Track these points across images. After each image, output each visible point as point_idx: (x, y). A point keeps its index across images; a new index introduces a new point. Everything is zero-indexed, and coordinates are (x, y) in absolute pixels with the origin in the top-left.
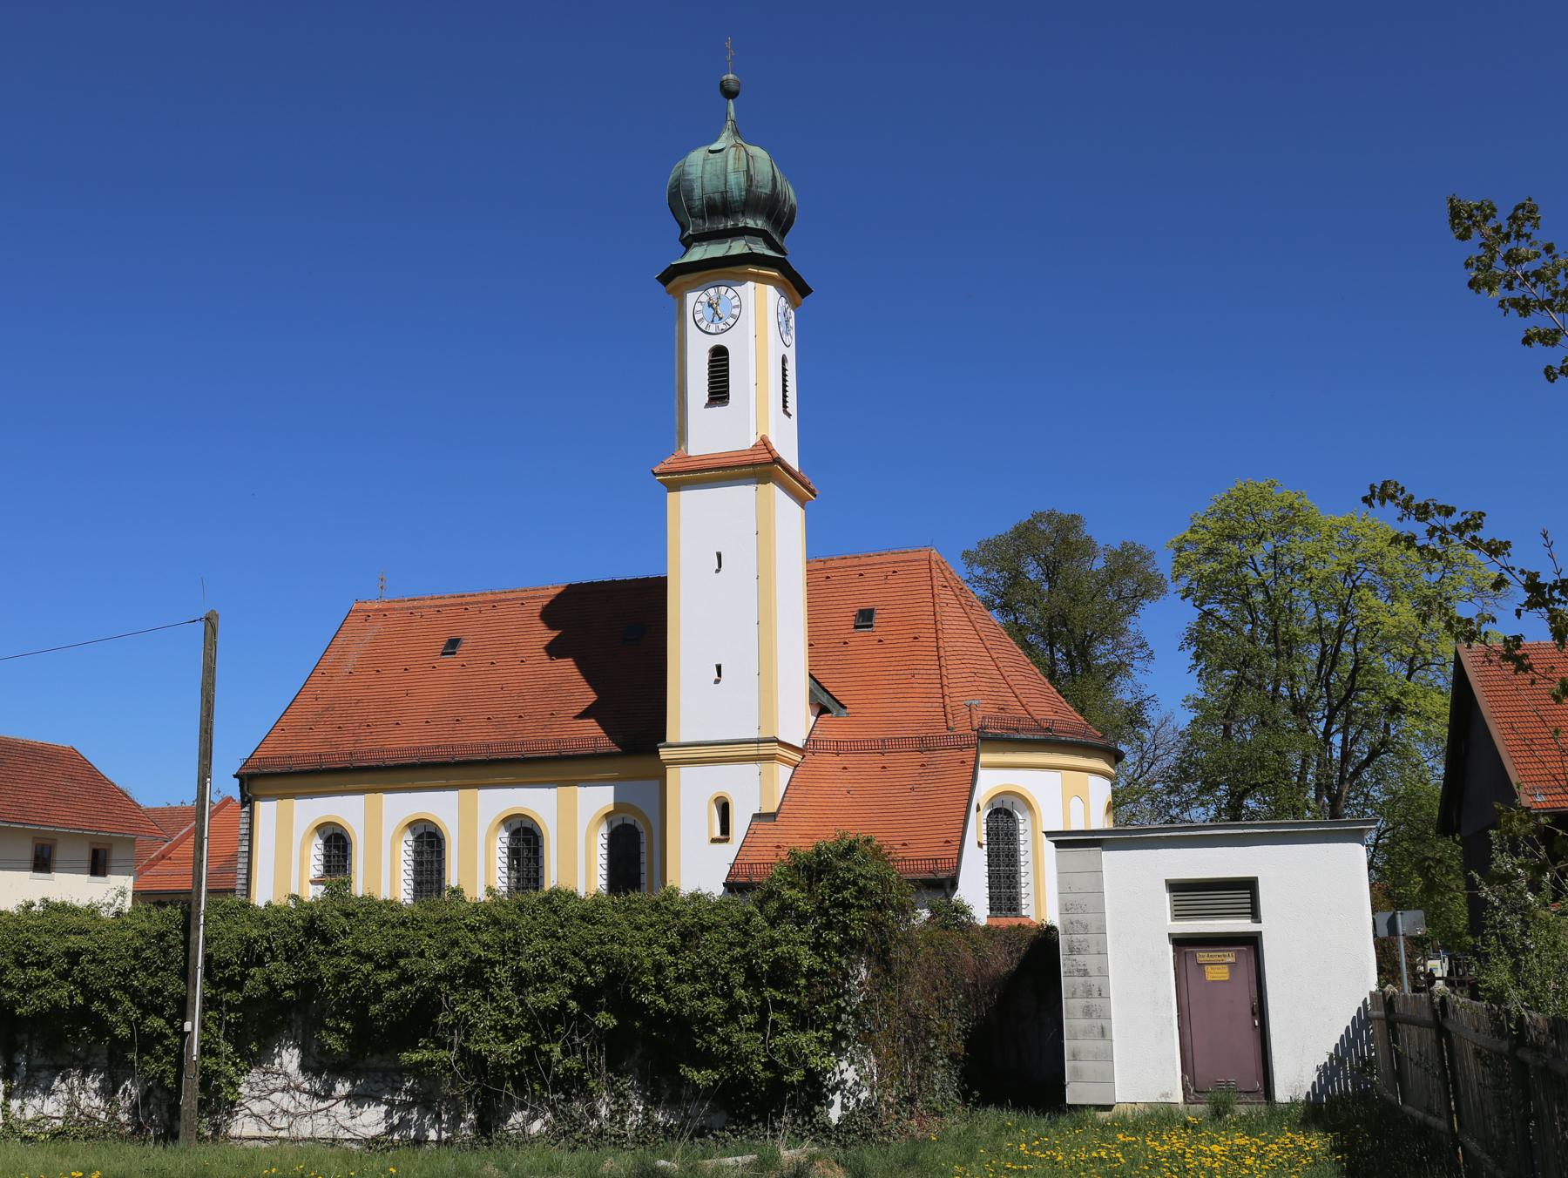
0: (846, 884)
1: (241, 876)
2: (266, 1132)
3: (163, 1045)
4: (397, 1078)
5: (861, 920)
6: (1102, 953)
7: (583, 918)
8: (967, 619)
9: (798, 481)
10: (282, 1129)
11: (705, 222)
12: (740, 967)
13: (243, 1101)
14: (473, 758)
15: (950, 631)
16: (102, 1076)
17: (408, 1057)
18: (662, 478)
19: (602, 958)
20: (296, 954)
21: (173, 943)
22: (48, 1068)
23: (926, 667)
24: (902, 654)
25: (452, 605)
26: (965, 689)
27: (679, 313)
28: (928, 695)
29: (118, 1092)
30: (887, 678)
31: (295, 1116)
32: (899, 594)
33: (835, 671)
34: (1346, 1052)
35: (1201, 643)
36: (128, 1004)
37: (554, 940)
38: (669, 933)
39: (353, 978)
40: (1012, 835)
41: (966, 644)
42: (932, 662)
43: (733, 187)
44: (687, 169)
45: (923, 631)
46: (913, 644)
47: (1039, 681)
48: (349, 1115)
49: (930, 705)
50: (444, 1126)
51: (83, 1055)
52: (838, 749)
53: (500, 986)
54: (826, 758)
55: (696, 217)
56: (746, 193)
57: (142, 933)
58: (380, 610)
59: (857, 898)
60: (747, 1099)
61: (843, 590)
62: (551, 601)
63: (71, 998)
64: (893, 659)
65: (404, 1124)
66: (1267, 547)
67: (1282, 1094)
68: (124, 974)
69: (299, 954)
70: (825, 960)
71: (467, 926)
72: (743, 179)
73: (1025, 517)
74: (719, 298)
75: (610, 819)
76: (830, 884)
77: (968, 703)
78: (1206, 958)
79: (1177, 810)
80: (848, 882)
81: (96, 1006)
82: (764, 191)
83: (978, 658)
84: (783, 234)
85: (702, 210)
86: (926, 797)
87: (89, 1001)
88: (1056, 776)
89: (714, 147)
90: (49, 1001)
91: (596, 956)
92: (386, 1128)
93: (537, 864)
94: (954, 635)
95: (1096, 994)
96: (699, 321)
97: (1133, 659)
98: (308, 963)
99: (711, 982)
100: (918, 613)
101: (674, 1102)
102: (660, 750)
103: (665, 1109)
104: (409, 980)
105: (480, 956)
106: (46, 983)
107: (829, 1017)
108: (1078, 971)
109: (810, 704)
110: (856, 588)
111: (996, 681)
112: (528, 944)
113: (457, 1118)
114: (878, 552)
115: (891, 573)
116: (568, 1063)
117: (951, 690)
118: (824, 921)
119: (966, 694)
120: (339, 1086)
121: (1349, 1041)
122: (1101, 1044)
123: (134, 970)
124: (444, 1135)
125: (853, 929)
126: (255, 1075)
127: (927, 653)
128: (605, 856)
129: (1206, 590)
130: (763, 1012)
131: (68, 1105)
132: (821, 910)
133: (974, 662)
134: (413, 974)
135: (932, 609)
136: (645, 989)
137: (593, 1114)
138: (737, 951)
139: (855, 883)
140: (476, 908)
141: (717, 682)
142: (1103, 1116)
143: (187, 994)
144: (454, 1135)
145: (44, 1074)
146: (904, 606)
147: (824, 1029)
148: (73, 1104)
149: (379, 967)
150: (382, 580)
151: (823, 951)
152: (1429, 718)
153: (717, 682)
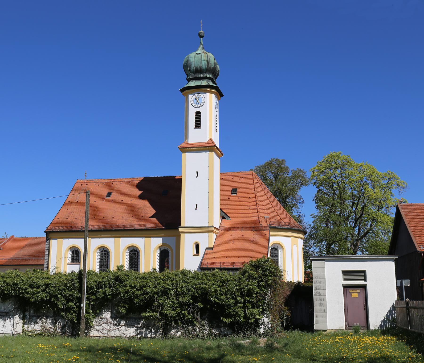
0: (266, 270)
1: (46, 262)
2: (101, 334)
3: (73, 310)
4: (139, 320)
5: (270, 279)
6: (325, 289)
7: (192, 277)
8: (264, 192)
9: (219, 151)
10: (105, 334)
12: (239, 291)
13: (94, 326)
14: (119, 229)
15: (259, 196)
16: (52, 319)
17: (144, 314)
19: (200, 288)
20: (112, 286)
21: (76, 282)
22: (36, 316)
23: (253, 206)
24: (246, 202)
25: (108, 182)
26: (264, 213)
27: (186, 101)
28: (254, 214)
29: (57, 323)
31: (109, 330)
33: (226, 206)
34: (389, 316)
35: (318, 199)
36: (62, 299)
38: (218, 282)
39: (129, 293)
40: (277, 255)
42: (255, 205)
44: (190, 59)
45: (251, 195)
46: (249, 199)
48: (125, 330)
49: (254, 217)
50: (153, 333)
51: (46, 313)
52: (229, 229)
53: (172, 295)
55: (192, 73)
57: (66, 279)
58: (86, 183)
59: (269, 274)
60: (238, 327)
62: (139, 182)
63: (46, 297)
64: (243, 204)
65: (141, 333)
66: (338, 171)
67: (372, 327)
68: (62, 291)
69: (113, 286)
70: (260, 290)
71: (161, 279)
72: (206, 63)
73: (269, 160)
76: (262, 270)
77: (265, 217)
79: (308, 248)
81: (53, 299)
84: (216, 79)
87: (51, 298)
89: (198, 52)
90: (40, 298)
92: (136, 334)
93: (138, 260)
95: (323, 300)
96: (192, 103)
98: (116, 289)
99: (231, 295)
101: (218, 327)
103: (215, 329)
104: (147, 294)
106: (39, 292)
107: (261, 305)
108: (318, 294)
110: (231, 182)
112: (179, 284)
113: (157, 331)
114: (237, 172)
116: (189, 316)
117: (260, 213)
119: (265, 214)
120: (122, 322)
121: (389, 314)
122: (324, 314)
123: (64, 290)
124: (153, 336)
125: (269, 282)
126: (97, 319)
129: (319, 184)
130: (244, 303)
131: (42, 327)
132: (260, 277)
133: (266, 205)
134: (148, 292)
135: (254, 189)
136: (212, 297)
137: (195, 330)
138: (238, 287)
141: (196, 209)
142: (325, 332)
143: (81, 296)
144: (156, 336)
145: (34, 318)
147: (260, 308)
148: (43, 326)
149: (137, 290)
151: (260, 287)
152: (384, 223)
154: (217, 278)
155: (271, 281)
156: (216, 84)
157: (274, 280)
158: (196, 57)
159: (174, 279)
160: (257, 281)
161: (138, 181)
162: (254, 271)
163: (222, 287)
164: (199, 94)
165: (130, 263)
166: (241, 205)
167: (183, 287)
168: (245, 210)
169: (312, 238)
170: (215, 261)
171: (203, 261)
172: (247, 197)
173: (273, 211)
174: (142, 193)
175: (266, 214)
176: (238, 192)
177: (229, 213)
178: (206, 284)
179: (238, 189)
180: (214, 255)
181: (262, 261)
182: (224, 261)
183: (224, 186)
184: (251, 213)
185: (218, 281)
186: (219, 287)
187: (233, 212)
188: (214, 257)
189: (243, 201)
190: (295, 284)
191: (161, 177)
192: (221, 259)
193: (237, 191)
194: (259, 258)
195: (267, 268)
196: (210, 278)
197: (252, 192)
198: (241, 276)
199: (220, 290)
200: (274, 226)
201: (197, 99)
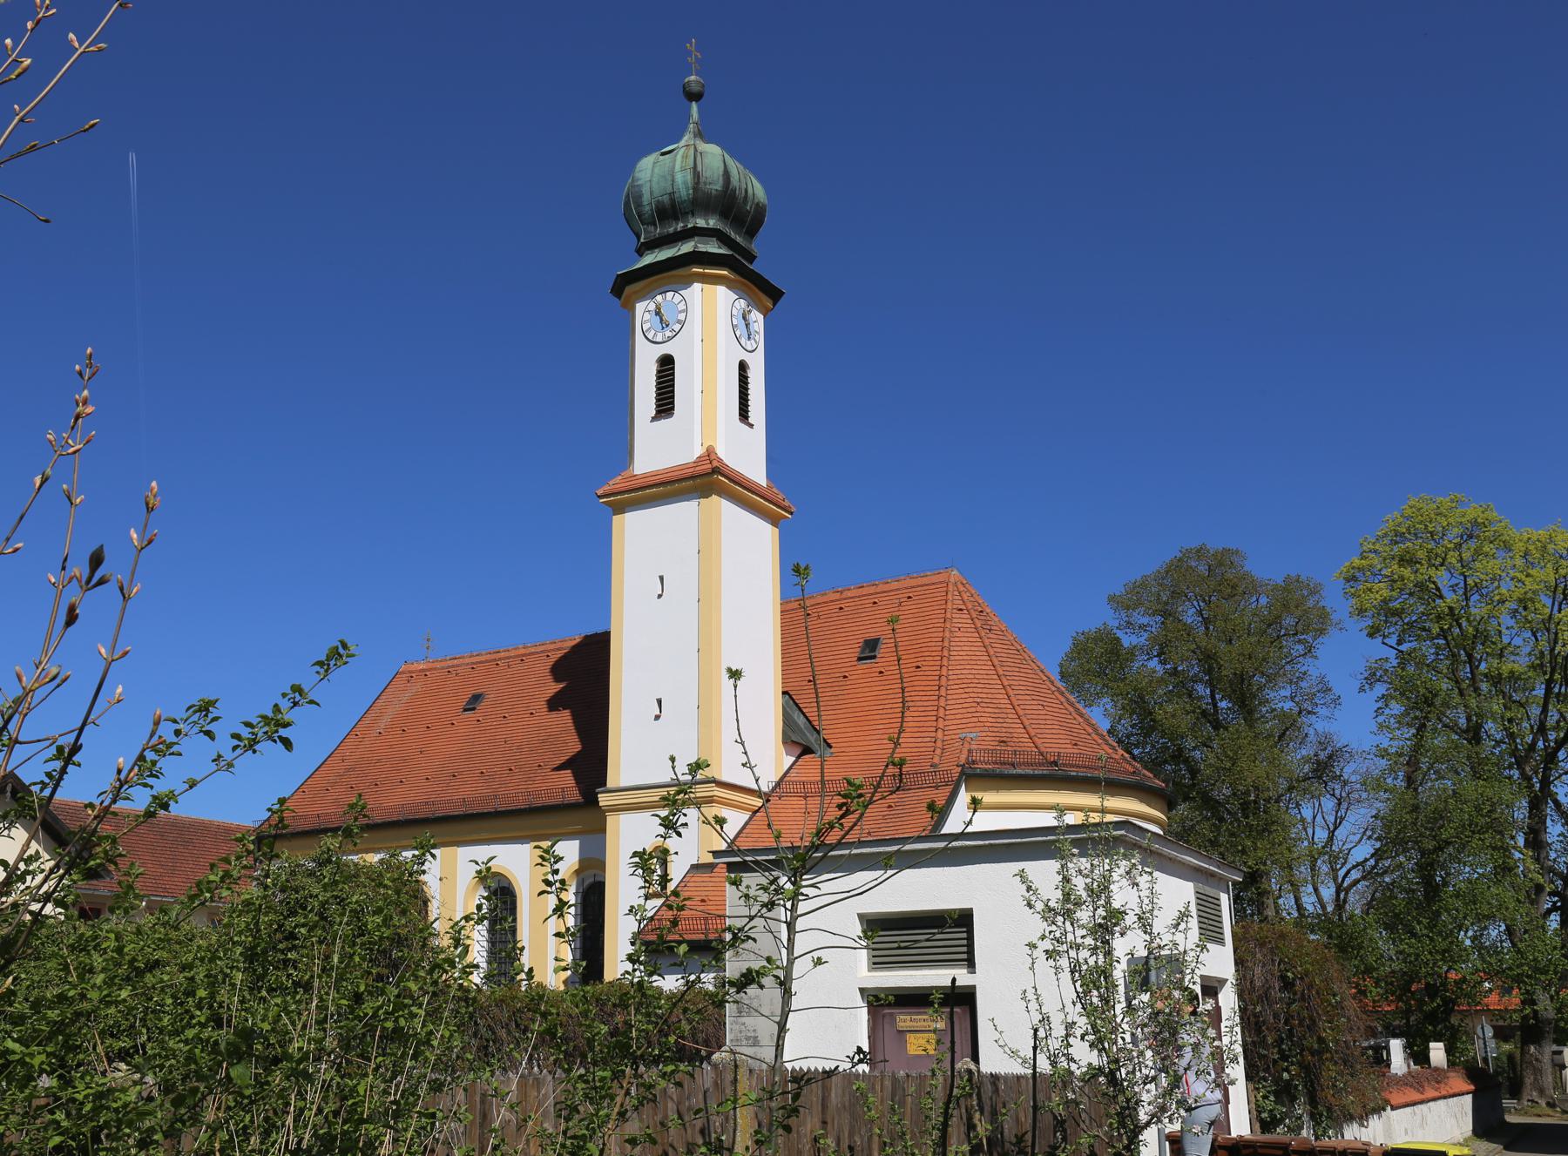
9: (753, 493)
11: (656, 229)
25: (487, 661)
26: (964, 721)
28: (921, 729)
30: (881, 712)
41: (974, 672)
55: (648, 224)
72: (689, 177)
75: (582, 876)
78: (908, 1023)
82: (715, 188)
108: (748, 1038)
109: (784, 743)
111: (1004, 711)
119: (964, 726)
133: (980, 690)
150: (428, 640)
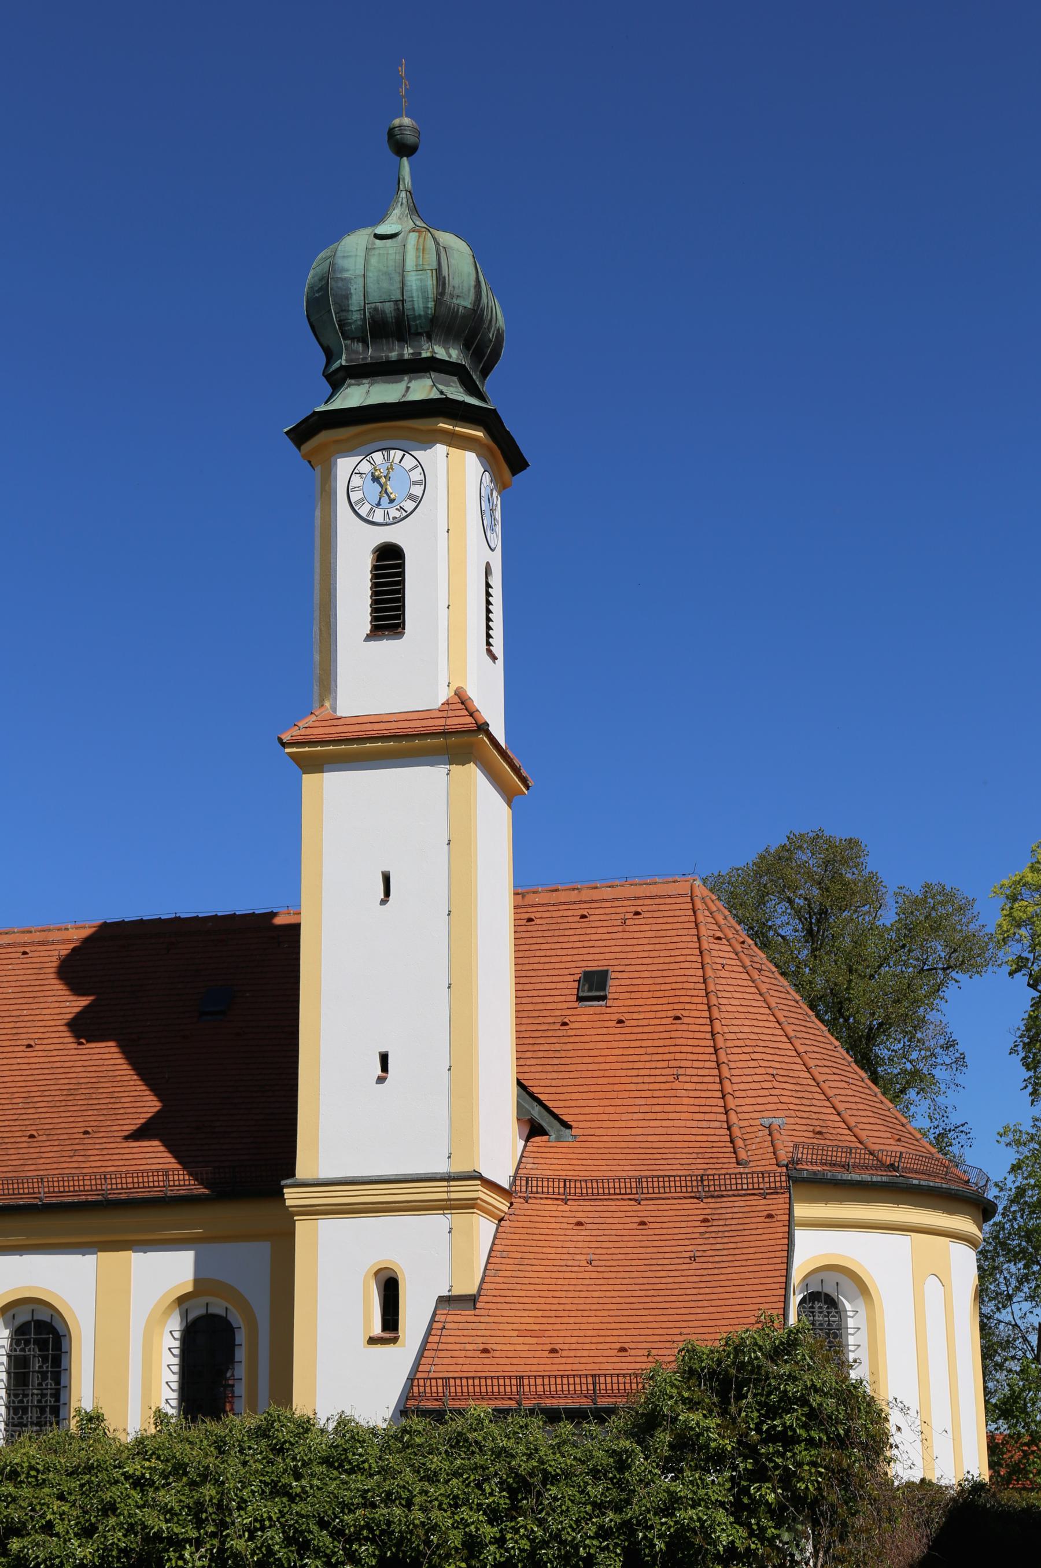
0: (787, 1403)
5: (813, 1464)
7: (327, 1461)
8: (754, 990)
12: (616, 1545)
15: (729, 1008)
18: (294, 750)
19: (371, 1530)
23: (696, 1064)
26: (760, 1100)
27: (323, 490)
28: (703, 1109)
32: (646, 948)
37: (285, 1500)
38: (486, 1486)
40: (836, 1336)
42: (707, 1057)
43: (415, 294)
44: (340, 262)
45: (687, 1006)
46: (674, 1027)
47: (867, 1091)
49: (705, 1124)
54: (547, 1208)
55: (352, 339)
56: (435, 305)
59: (805, 1426)
61: (555, 939)
62: (73, 950)
70: (752, 1534)
71: (127, 1476)
72: (430, 283)
73: (776, 841)
74: (390, 468)
75: (186, 1305)
76: (759, 1403)
80: (791, 1401)
83: (777, 1051)
84: (485, 373)
85: (363, 328)
86: (716, 1271)
88: (904, 1241)
89: (383, 229)
91: (362, 1528)
93: (58, 1383)
94: (737, 1015)
96: (357, 503)
97: (934, 1066)
100: (679, 979)
102: (285, 1190)
105: (161, 1531)
109: (518, 1119)
110: (576, 938)
112: (239, 1508)
114: (610, 883)
115: (631, 915)
117: (738, 1102)
118: (749, 1467)
125: (801, 1479)
127: (696, 1042)
128: (176, 1369)
132: (748, 1450)
133: (770, 1057)
135: (700, 972)
138: (611, 1518)
139: (804, 1401)
140: (141, 1448)
141: (381, 1080)
146: (655, 967)
151: (749, 1517)
153: (381, 1080)
154: (478, 1459)
155: (820, 1474)
156: (481, 397)
157: (833, 1465)
158: (377, 252)
159: (205, 1476)
160: (727, 1474)
161: (70, 941)
162: (711, 1411)
163: (513, 1519)
164: (392, 452)
165: (16, 1396)
166: (631, 1058)
167: (262, 1521)
168: (651, 1087)
169: (1014, 1256)
170: (487, 1368)
171: (419, 1375)
172: (664, 1014)
173: (809, 1088)
174: (86, 1007)
175: (769, 1107)
176: (613, 989)
177: (568, 1103)
178: (409, 1504)
179: (614, 975)
180: (483, 1340)
181: (760, 1349)
182: (541, 1368)
183: (536, 960)
184: (685, 1101)
185: (487, 1479)
186: (490, 1522)
187: (591, 1096)
188: (485, 1351)
189: (640, 1036)
190: (953, 1499)
191: (196, 919)
192: (523, 1361)
193: (610, 982)
194: (740, 1329)
195: (791, 1388)
196: (435, 1462)
197: (692, 986)
198: (626, 1444)
199: (501, 1541)
200: (815, 1168)
201: (383, 480)
